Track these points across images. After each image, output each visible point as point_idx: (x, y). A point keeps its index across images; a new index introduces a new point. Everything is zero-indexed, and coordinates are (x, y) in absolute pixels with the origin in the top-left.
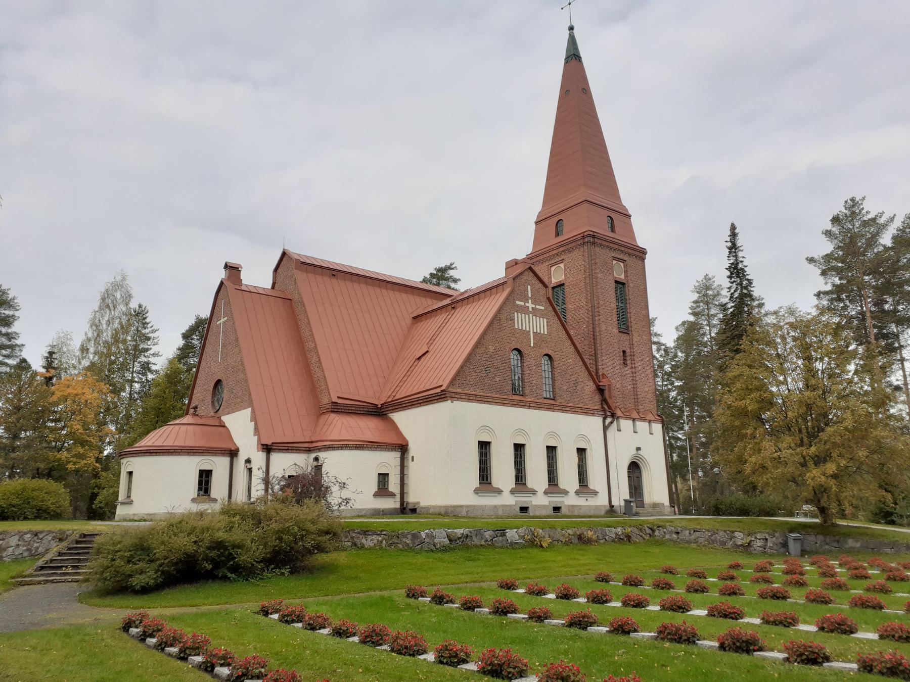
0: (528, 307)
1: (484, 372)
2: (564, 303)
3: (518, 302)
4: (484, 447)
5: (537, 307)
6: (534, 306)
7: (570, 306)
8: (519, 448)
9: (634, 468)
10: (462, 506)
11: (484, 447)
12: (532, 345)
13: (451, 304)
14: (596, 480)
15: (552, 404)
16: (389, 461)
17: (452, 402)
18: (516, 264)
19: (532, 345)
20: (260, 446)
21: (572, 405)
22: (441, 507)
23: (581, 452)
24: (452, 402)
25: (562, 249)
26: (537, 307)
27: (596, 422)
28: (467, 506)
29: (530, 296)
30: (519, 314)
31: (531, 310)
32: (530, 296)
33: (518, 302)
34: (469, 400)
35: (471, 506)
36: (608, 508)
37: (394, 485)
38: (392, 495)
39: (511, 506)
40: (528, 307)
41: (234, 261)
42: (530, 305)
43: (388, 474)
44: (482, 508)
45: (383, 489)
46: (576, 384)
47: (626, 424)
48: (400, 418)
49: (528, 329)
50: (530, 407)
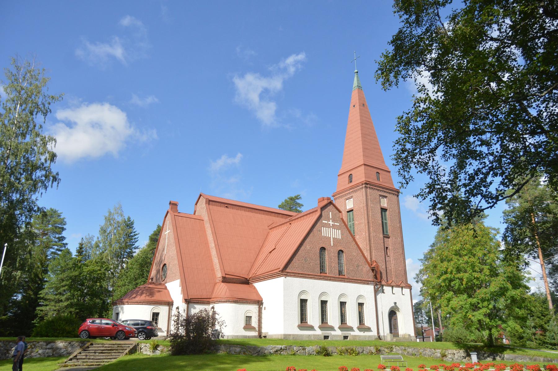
0: (330, 224)
1: (304, 260)
2: (353, 221)
3: (324, 221)
4: (303, 303)
5: (335, 224)
6: (333, 223)
7: (356, 222)
8: (324, 303)
9: (392, 314)
10: (290, 335)
11: (303, 303)
12: (332, 245)
13: (289, 222)
14: (369, 321)
15: (340, 277)
16: (253, 309)
17: (285, 278)
18: (323, 200)
19: (332, 245)
20: (184, 300)
21: (355, 278)
22: (279, 335)
23: (361, 305)
24: (285, 278)
25: (351, 190)
26: (335, 224)
27: (369, 289)
28: (293, 335)
29: (331, 217)
30: (325, 228)
31: (331, 225)
32: (331, 217)
33: (324, 221)
34: (295, 276)
35: (296, 335)
36: (377, 337)
37: (254, 323)
38: (253, 329)
39: (318, 335)
40: (330, 224)
41: (174, 200)
42: (331, 223)
43: (251, 317)
44: (301, 335)
45: (248, 326)
46: (358, 266)
47: (387, 289)
48: (259, 286)
49: (329, 236)
50: (330, 280)
